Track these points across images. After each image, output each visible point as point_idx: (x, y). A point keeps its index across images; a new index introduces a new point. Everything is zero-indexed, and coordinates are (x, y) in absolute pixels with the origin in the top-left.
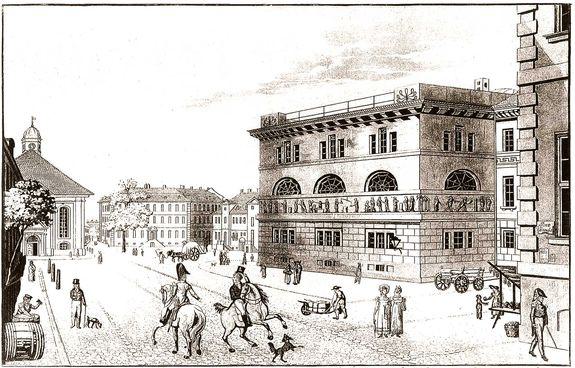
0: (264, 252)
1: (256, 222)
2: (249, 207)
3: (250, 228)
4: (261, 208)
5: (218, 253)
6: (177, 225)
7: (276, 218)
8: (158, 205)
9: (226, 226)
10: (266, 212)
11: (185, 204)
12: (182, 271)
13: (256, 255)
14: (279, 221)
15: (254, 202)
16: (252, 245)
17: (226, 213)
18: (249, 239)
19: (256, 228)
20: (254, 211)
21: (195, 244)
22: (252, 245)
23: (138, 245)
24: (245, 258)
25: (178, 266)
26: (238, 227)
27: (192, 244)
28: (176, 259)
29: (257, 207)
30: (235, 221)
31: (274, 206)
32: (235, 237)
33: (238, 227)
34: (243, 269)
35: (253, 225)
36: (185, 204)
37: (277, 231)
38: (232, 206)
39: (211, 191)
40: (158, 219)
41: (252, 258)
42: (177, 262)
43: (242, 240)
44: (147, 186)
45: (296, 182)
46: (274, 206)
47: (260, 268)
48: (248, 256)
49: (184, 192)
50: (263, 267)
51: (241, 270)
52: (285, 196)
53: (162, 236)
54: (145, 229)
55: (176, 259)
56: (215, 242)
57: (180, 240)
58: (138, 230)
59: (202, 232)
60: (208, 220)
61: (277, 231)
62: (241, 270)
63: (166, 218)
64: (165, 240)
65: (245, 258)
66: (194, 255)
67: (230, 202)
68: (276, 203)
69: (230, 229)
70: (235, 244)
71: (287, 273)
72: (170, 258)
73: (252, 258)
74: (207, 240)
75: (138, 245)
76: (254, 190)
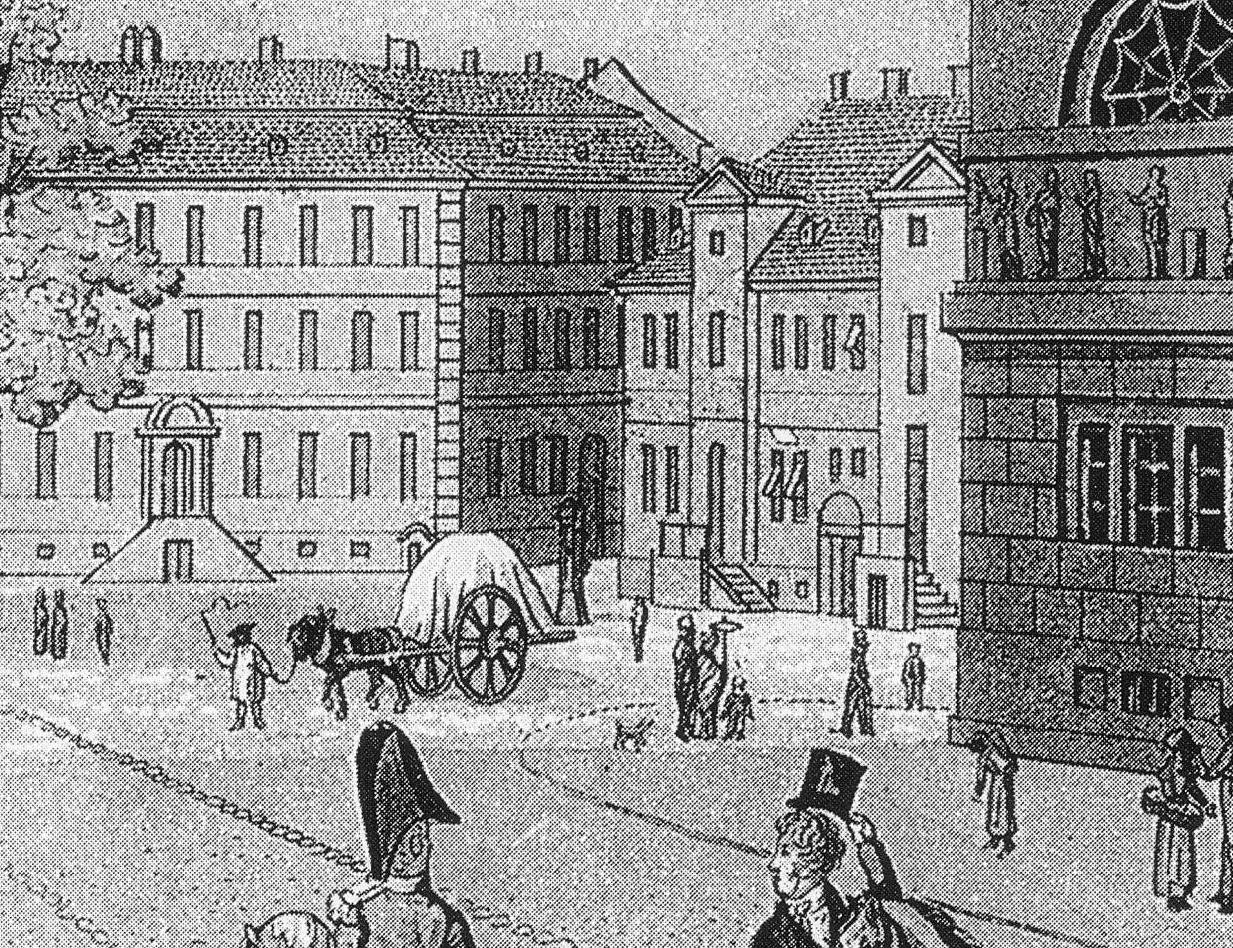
0: (995, 628)
1: (945, 351)
2: (894, 222)
3: (900, 410)
4: (977, 231)
5: (663, 638)
6: (370, 278)
7: (1090, 315)
8: (224, 209)
9: (720, 389)
10: (1011, 267)
11: (426, 201)
12: (399, 795)
13: (941, 651)
14: (1120, 349)
15: (931, 177)
16: (915, 556)
17: (717, 281)
18: (894, 508)
19: (944, 410)
20: (927, 265)
21: (496, 553)
22: (915, 556)
23: (74, 557)
24: (859, 686)
25: (370, 744)
26: (807, 402)
27: (472, 558)
28: (357, 682)
29: (949, 226)
30: (788, 347)
31: (1071, 216)
32: (787, 495)
33: (807, 402)
34: (849, 773)
35: (917, 384)
36: (426, 201)
37: (1097, 438)
38: (765, 219)
39: (611, 85)
40: (223, 339)
41: (915, 674)
42: (363, 719)
43: (841, 511)
44: (141, 38)
45: (922, 673)
46: (1071, 216)
47: (967, 766)
48: (888, 654)
49: (419, 108)
50: (995, 742)
51: (831, 783)
52: (1154, 132)
53: (252, 484)
54: (125, 422)
55: (357, 682)
56: (639, 529)
57: (384, 512)
58: (77, 424)
59: (545, 460)
60: (591, 340)
61: (1097, 438)
62: (831, 783)
63: (281, 320)
64: (277, 518)
65: (859, 686)
66: (489, 649)
67: (751, 184)
68: (1092, 199)
69: (750, 423)
70: (787, 546)
71: (1175, 812)
72: (312, 675)
73: (915, 674)
74: (582, 526)
75: (74, 557)
76: (928, 80)
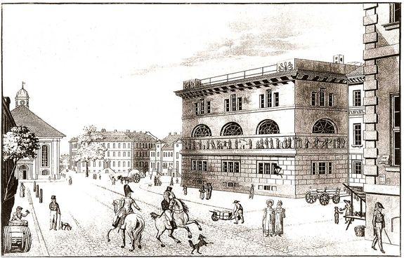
0: (186, 177)
1: (180, 156)
2: (175, 145)
3: (176, 160)
4: (183, 146)
5: (153, 178)
6: (125, 158)
7: (194, 153)
8: (111, 144)
9: (159, 158)
10: (187, 148)
11: (130, 143)
12: (128, 190)
13: (180, 179)
14: (196, 155)
15: (179, 141)
16: (177, 172)
17: (158, 150)
18: (175, 167)
19: (180, 160)
20: (179, 148)
21: (137, 171)
22: (177, 172)
23: (97, 171)
24: (172, 181)
25: (125, 186)
26: (167, 159)
27: (135, 171)
28: (124, 181)
29: (180, 145)
30: (165, 155)
31: (192, 144)
32: (165, 166)
33: (167, 159)
34: (171, 189)
35: (177, 158)
36: (130, 143)
37: (195, 162)
38: (163, 145)
39: (148, 134)
40: (111, 153)
41: (177, 181)
42: (124, 184)
43: (170, 168)
44: (104, 130)
45: (208, 128)
46: (192, 144)
47: (182, 188)
48: (174, 179)
49: (129, 135)
50: (185, 187)
51: (169, 189)
52: (200, 138)
53: (114, 165)
54: (102, 161)
55: (124, 181)
56: (151, 169)
57: (127, 168)
58: (97, 161)
59: (142, 163)
60: (146, 154)
61: (195, 162)
62: (169, 189)
63: (117, 153)
64: (116, 168)
65: (172, 181)
66: (137, 179)
67: (162, 142)
68: (194, 143)
69: (161, 161)
70: (165, 171)
71: (202, 192)
72: (120, 181)
73: (177, 181)
74: (146, 169)
75: (97, 171)
76: (179, 133)
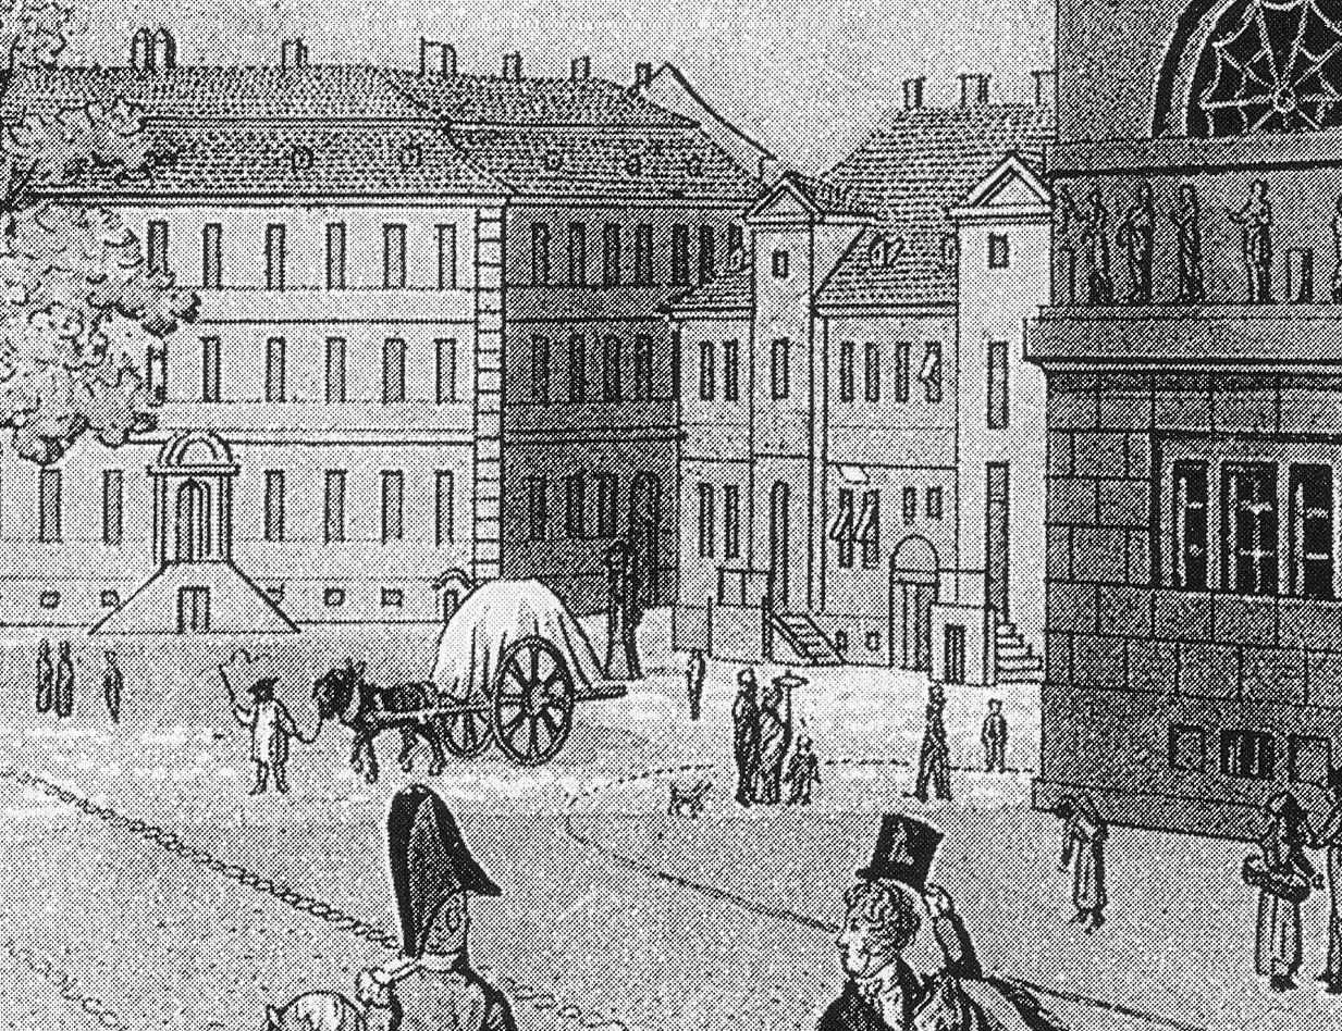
0: (1083, 683)
1: (1028, 382)
2: (973, 241)
3: (980, 446)
4: (1063, 251)
5: (721, 694)
6: (403, 302)
7: (1187, 343)
8: (244, 227)
9: (784, 423)
10: (1101, 291)
11: (464, 219)
12: (434, 864)
13: (1024, 708)
14: (1219, 379)
15: (1014, 192)
16: (996, 604)
17: (781, 305)
18: (973, 553)
19: (1028, 446)
20: (1009, 288)
21: (540, 601)
22: (996, 604)
23: (80, 606)
24: (935, 746)
25: (403, 809)
26: (878, 437)
27: (514, 607)
28: (388, 741)
29: (1032, 246)
30: (858, 378)
31: (1166, 235)
32: (856, 538)
33: (878, 437)
34: (924, 841)
35: (998, 418)
36: (464, 219)
37: (1194, 476)
38: (833, 238)
39: (665, 92)
40: (243, 369)
41: (996, 733)
42: (395, 782)
43: (915, 556)
44: (154, 41)
45: (1003, 731)
46: (1166, 235)
47: (1053, 833)
48: (966, 711)
49: (456, 117)
50: (1083, 807)
51: (904, 851)
52: (1256, 144)
53: (275, 527)
54: (136, 459)
55: (388, 741)
56: (695, 575)
57: (418, 556)
58: (84, 461)
59: (593, 500)
60: (643, 369)
61: (1194, 476)
62: (904, 851)
63: (306, 348)
64: (302, 564)
65: (935, 746)
66: (533, 706)
67: (817, 200)
68: (1188, 217)
69: (817, 460)
70: (856, 594)
71: (1278, 883)
72: (340, 735)
73: (996, 733)
74: (633, 572)
75: (80, 606)
76: (1010, 87)
